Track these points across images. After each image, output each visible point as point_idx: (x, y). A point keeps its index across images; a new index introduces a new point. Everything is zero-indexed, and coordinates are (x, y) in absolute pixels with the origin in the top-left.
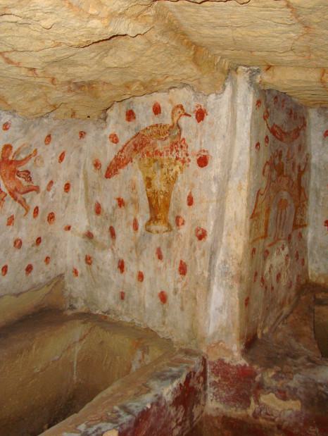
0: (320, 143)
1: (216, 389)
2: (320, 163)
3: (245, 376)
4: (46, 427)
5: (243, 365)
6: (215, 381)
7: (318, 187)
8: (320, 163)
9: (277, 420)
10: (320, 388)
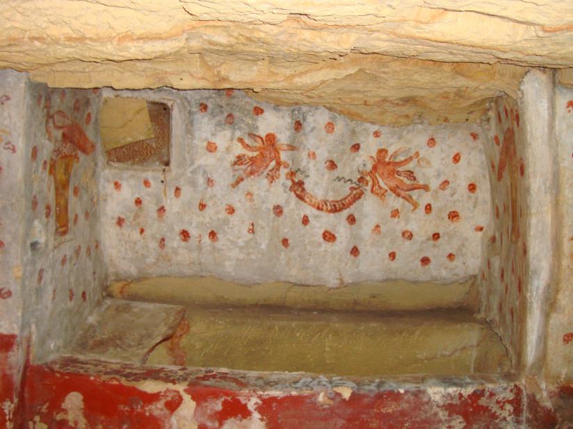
5: (549, 409)
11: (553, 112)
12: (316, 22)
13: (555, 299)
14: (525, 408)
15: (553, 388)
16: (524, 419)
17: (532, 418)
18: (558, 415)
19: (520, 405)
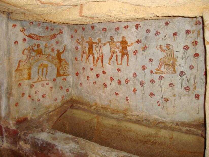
0: (70, 40)
1: (7, 138)
2: (72, 49)
3: (15, 133)
4: (87, 139)
5: (14, 129)
6: (6, 135)
7: (72, 59)
8: (72, 49)
9: (25, 152)
10: (35, 140)
11: (8, 28)
12: (92, 61)
13: (11, 93)
14: (4, 132)
15: (14, 122)
16: (4, 136)
17: (8, 135)
18: (18, 130)
19: (2, 132)
